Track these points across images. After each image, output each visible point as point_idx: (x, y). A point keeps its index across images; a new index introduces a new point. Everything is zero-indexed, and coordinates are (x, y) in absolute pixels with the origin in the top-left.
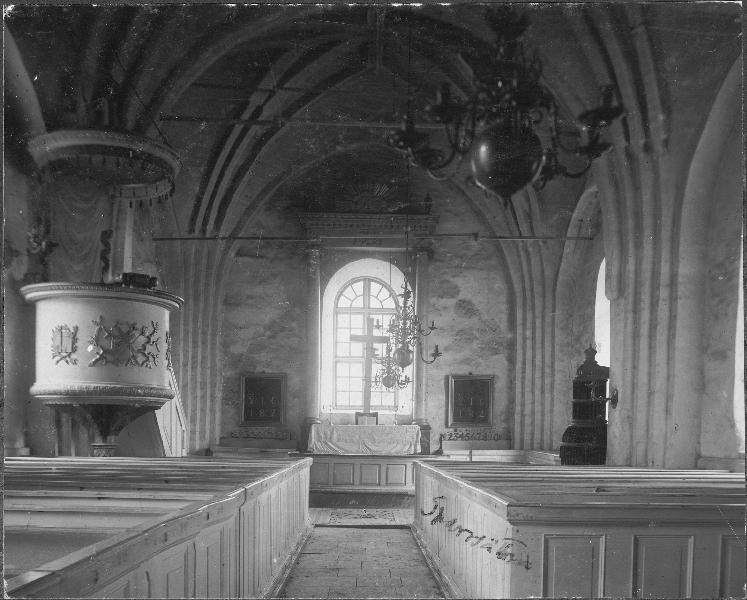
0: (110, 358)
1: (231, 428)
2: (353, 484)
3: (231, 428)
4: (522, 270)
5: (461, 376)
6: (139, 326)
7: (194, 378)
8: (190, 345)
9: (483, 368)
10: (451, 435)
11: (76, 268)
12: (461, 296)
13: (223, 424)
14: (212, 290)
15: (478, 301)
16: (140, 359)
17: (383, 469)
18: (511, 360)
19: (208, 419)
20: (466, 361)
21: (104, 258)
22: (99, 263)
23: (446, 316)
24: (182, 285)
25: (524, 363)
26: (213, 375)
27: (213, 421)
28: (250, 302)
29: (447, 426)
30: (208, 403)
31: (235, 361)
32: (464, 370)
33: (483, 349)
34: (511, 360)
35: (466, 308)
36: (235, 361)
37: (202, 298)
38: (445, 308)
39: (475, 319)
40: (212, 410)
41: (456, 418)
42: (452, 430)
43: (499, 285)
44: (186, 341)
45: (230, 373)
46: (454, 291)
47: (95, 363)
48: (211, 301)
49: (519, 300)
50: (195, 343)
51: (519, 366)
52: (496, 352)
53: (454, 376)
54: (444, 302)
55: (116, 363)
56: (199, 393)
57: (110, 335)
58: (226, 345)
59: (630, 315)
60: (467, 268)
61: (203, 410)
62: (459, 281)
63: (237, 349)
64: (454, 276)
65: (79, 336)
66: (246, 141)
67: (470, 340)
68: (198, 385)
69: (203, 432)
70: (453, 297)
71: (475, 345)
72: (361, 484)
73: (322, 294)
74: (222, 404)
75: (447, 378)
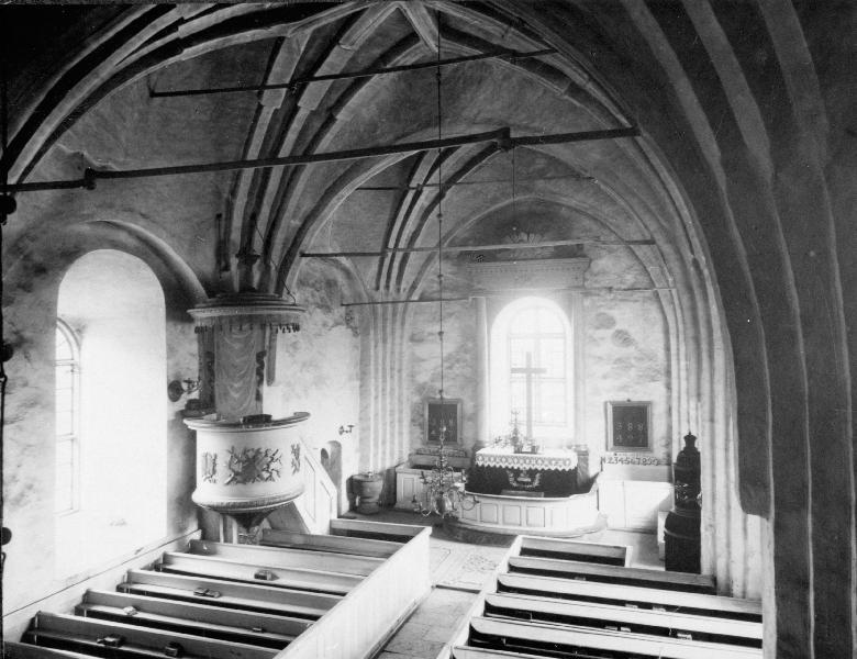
0: (239, 478)
1: (418, 445)
2: (497, 523)
3: (418, 445)
4: (673, 303)
5: (618, 403)
6: (263, 450)
7: (384, 409)
8: (380, 380)
9: (637, 396)
10: (611, 459)
11: (236, 385)
12: (618, 327)
13: (412, 442)
14: (398, 333)
15: (635, 332)
16: (265, 475)
17: (524, 512)
18: (669, 387)
19: (396, 441)
20: (624, 388)
21: (260, 374)
22: (255, 378)
23: (607, 347)
24: (372, 332)
25: (679, 392)
26: (400, 402)
27: (401, 444)
28: (430, 338)
29: (607, 449)
30: (397, 427)
31: (421, 389)
32: (622, 397)
33: (641, 376)
34: (669, 387)
35: (624, 338)
36: (421, 389)
37: (389, 340)
38: (602, 339)
39: (631, 350)
40: (401, 434)
41: (616, 443)
42: (612, 453)
43: (655, 314)
44: (376, 378)
45: (417, 399)
46: (610, 322)
47: (228, 483)
48: (397, 341)
49: (672, 331)
50: (384, 377)
51: (675, 394)
52: (653, 380)
53: (612, 403)
54: (602, 333)
55: (244, 481)
56: (388, 420)
57: (239, 462)
58: (412, 376)
59: (707, 425)
60: (622, 300)
61: (392, 435)
62: (615, 313)
63: (423, 378)
64: (610, 308)
65: (218, 461)
66: (417, 208)
67: (628, 367)
68: (388, 413)
69: (392, 454)
70: (608, 328)
71: (633, 372)
72: (504, 523)
73: (489, 333)
74: (410, 426)
75: (606, 403)
